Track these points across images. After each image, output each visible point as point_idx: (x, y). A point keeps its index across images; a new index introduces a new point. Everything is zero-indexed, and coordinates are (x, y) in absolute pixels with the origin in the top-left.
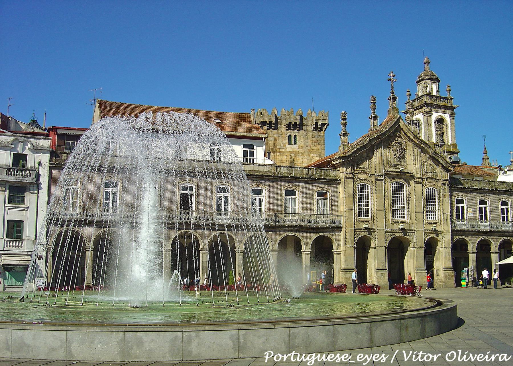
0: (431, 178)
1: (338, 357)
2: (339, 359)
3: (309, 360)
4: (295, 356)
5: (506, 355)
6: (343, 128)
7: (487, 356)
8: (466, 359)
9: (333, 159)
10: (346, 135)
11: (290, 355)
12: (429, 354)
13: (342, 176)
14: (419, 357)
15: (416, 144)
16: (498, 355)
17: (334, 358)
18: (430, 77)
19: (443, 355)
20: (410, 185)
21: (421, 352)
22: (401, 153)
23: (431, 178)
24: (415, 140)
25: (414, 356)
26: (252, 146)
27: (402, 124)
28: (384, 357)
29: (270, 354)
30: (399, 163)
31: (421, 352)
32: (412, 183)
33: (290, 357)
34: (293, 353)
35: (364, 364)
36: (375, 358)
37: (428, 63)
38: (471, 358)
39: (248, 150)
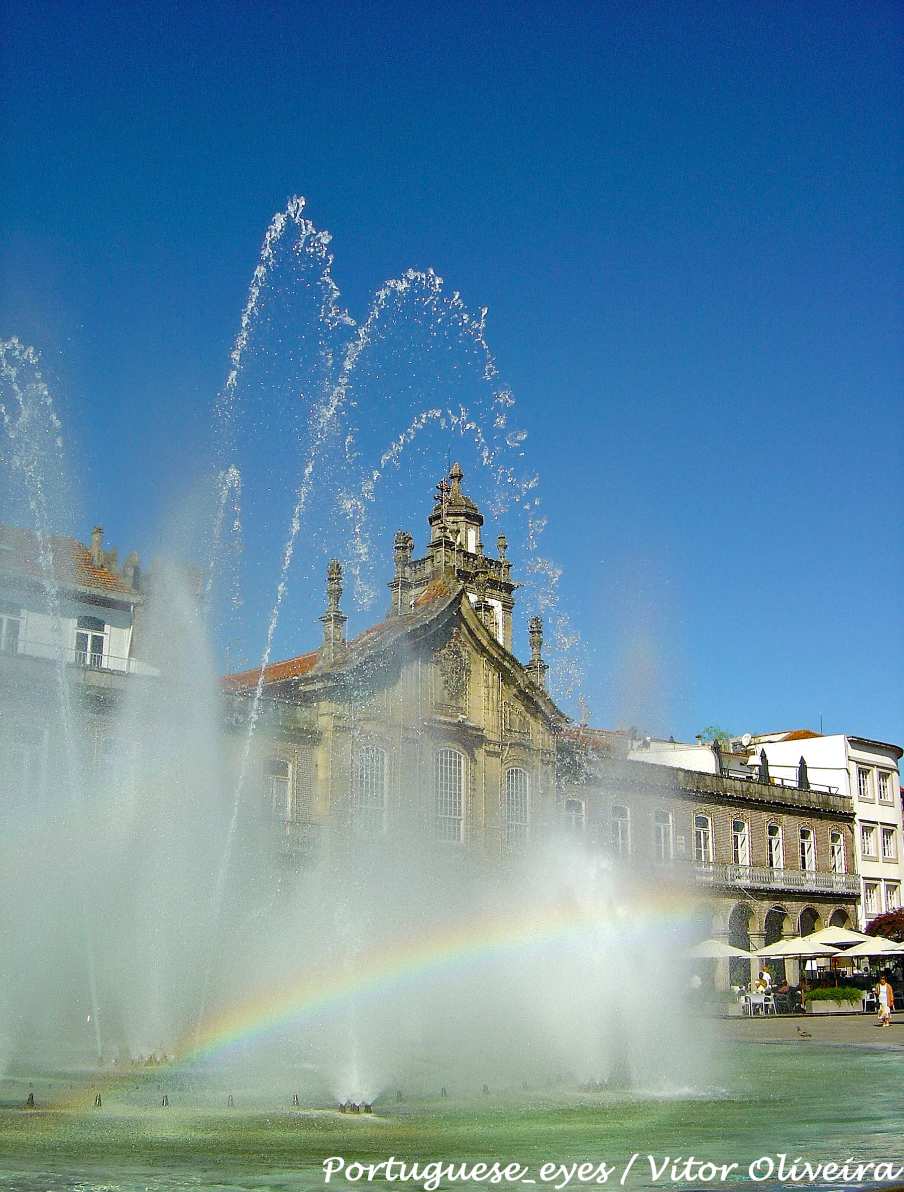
0: (520, 745)
1: (497, 1171)
2: (499, 1175)
3: (427, 1177)
4: (395, 1170)
5: (890, 1166)
6: (332, 601)
7: (846, 1169)
8: (797, 1175)
9: (307, 679)
10: (340, 620)
11: (382, 1165)
12: (710, 1165)
13: (324, 722)
14: (687, 1172)
15: (491, 659)
16: (872, 1165)
17: (593, 1172)
18: (463, 510)
19: (744, 1167)
20: (473, 759)
21: (692, 1159)
22: (460, 679)
23: (520, 745)
24: (491, 650)
25: (674, 1168)
26: (98, 625)
27: (465, 608)
28: (603, 1171)
29: (336, 1164)
30: (453, 703)
31: (692, 1159)
32: (480, 754)
33: (383, 1170)
34: (391, 1162)
35: (557, 1187)
36: (582, 1172)
37: (460, 477)
38: (807, 1174)
39: (90, 634)
